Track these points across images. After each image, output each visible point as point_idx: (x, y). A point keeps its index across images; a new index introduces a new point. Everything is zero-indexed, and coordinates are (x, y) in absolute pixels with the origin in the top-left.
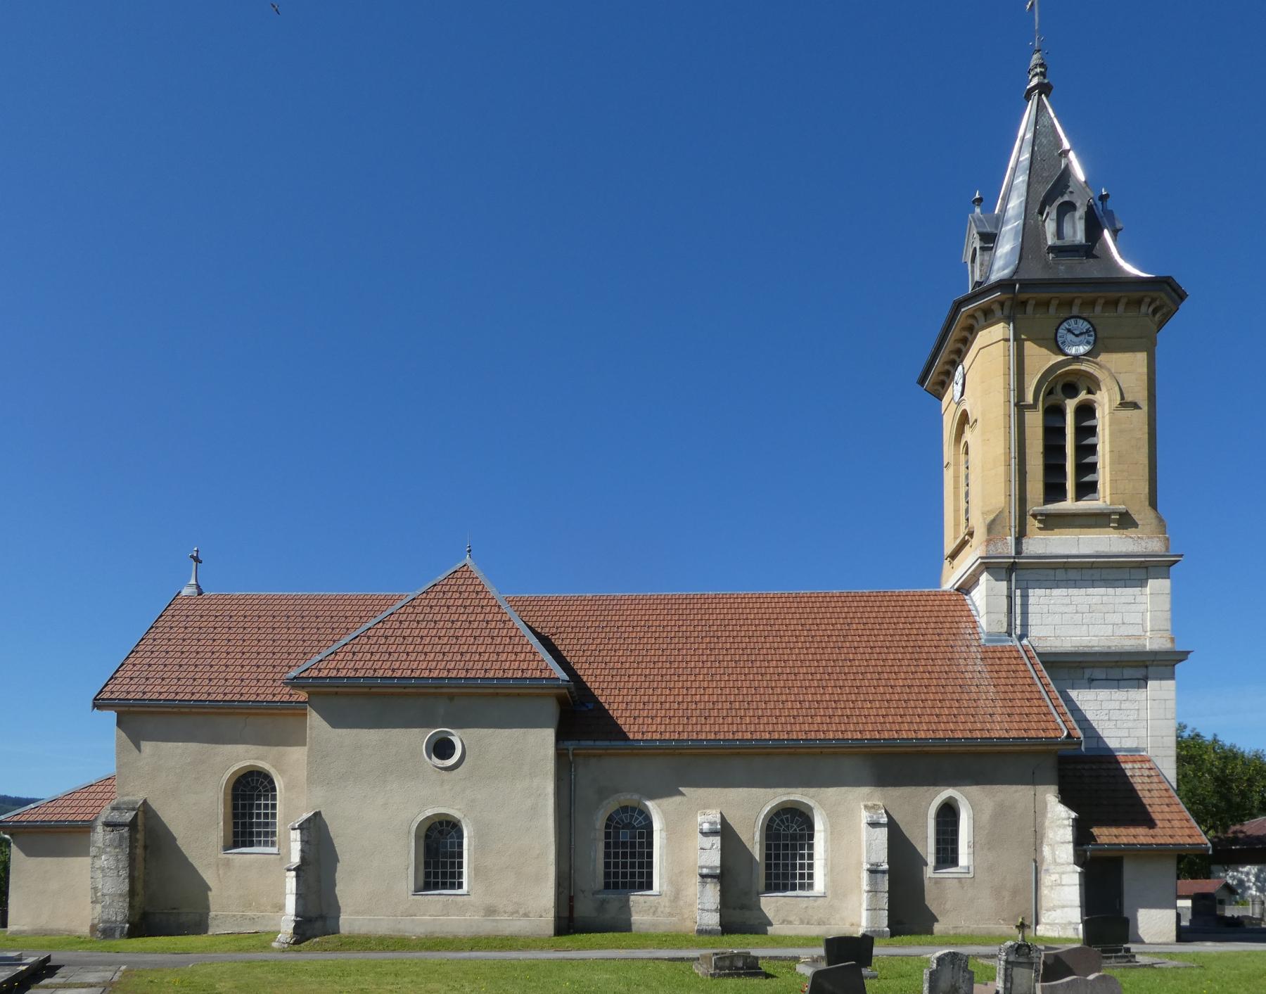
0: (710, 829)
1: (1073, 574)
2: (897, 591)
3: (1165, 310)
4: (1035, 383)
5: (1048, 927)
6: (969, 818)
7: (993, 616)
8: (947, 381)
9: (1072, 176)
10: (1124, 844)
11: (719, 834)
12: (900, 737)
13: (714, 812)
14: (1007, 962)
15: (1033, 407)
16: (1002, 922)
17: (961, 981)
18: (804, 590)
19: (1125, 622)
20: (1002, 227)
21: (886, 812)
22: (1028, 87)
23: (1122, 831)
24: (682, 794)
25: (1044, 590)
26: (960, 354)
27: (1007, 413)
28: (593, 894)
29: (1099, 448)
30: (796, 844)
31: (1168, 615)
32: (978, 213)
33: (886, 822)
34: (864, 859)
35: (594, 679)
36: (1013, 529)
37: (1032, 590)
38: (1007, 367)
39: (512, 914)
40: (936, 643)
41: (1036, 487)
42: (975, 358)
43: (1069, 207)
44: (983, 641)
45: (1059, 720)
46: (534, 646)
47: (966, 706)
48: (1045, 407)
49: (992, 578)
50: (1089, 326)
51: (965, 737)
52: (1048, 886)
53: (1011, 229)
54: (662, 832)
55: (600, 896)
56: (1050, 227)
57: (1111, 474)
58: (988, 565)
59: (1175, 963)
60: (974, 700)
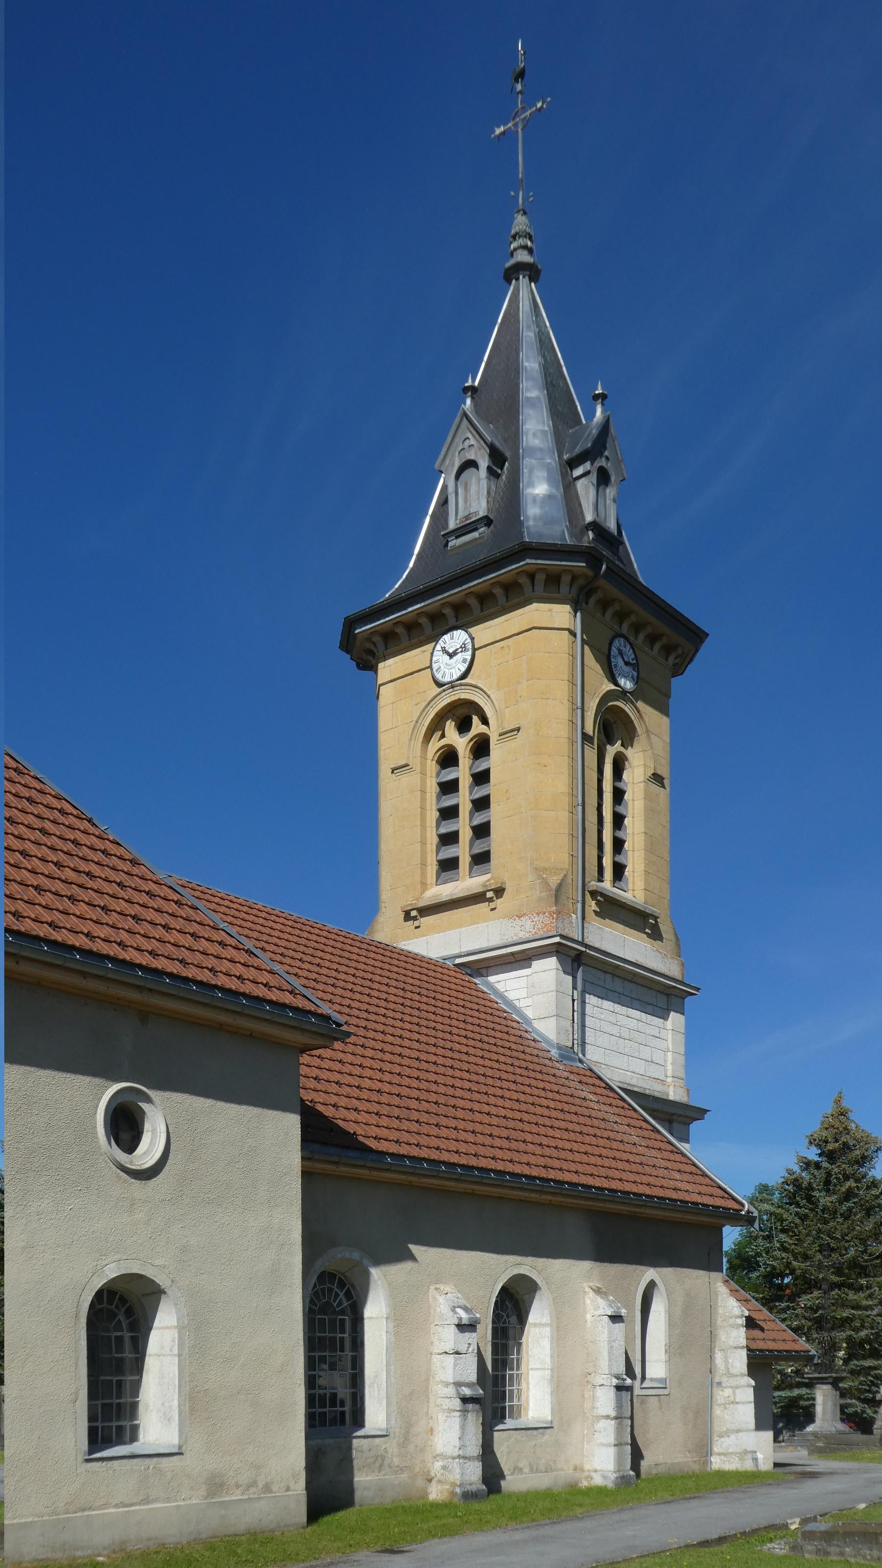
24: (412, 1258)
52: (721, 1405)
54: (389, 1321)
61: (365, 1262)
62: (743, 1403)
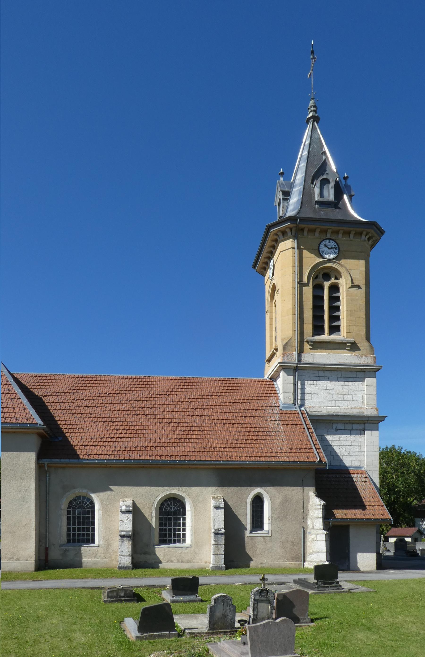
0: (126, 510)
1: (328, 374)
2: (239, 378)
3: (374, 239)
4: (308, 272)
5: (310, 563)
6: (269, 504)
7: (287, 395)
8: (267, 268)
9: (328, 165)
10: (349, 519)
11: (131, 512)
12: (232, 460)
13: (129, 500)
14: (255, 600)
15: (307, 284)
16: (286, 561)
17: (228, 611)
18: (189, 376)
19: (354, 400)
20: (293, 189)
21: (224, 501)
22: (308, 117)
23: (349, 511)
24: (111, 490)
25: (313, 381)
26: (272, 253)
27: (294, 287)
28: (60, 546)
29: (341, 308)
30: (176, 517)
31: (375, 397)
32: (281, 180)
33: (223, 506)
34: (212, 527)
35: (64, 423)
36: (296, 349)
37: (307, 381)
38: (294, 262)
39: (10, 559)
40: (256, 408)
41: (308, 327)
42: (278, 256)
43: (325, 182)
44: (281, 407)
45: (316, 452)
46: (25, 405)
47: (268, 443)
48: (314, 285)
49: (286, 374)
50: (335, 244)
51: (266, 460)
52: (310, 541)
53: (297, 190)
55: (63, 548)
56: (317, 191)
57: (347, 322)
58: (283, 367)
59: (363, 589)
60: (273, 440)
61: (89, 492)
62: (320, 541)
